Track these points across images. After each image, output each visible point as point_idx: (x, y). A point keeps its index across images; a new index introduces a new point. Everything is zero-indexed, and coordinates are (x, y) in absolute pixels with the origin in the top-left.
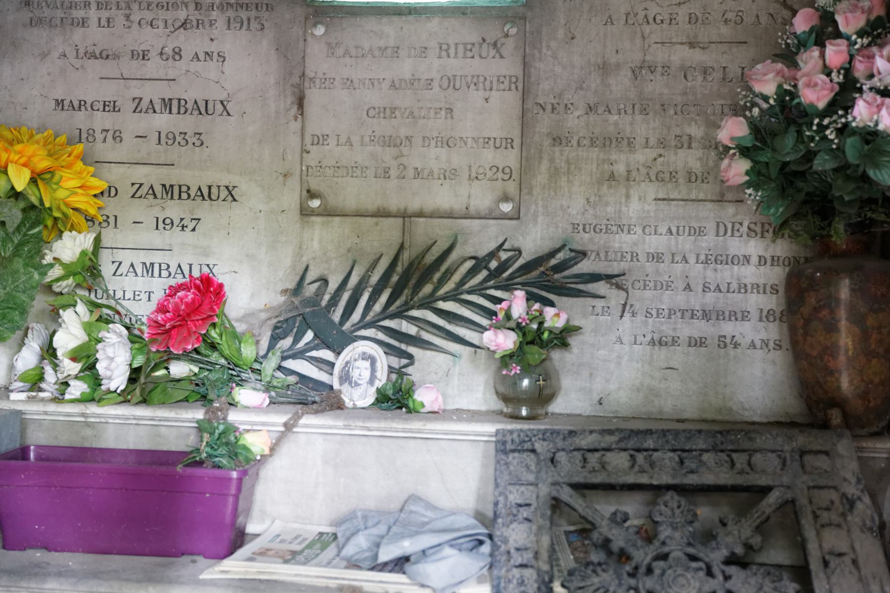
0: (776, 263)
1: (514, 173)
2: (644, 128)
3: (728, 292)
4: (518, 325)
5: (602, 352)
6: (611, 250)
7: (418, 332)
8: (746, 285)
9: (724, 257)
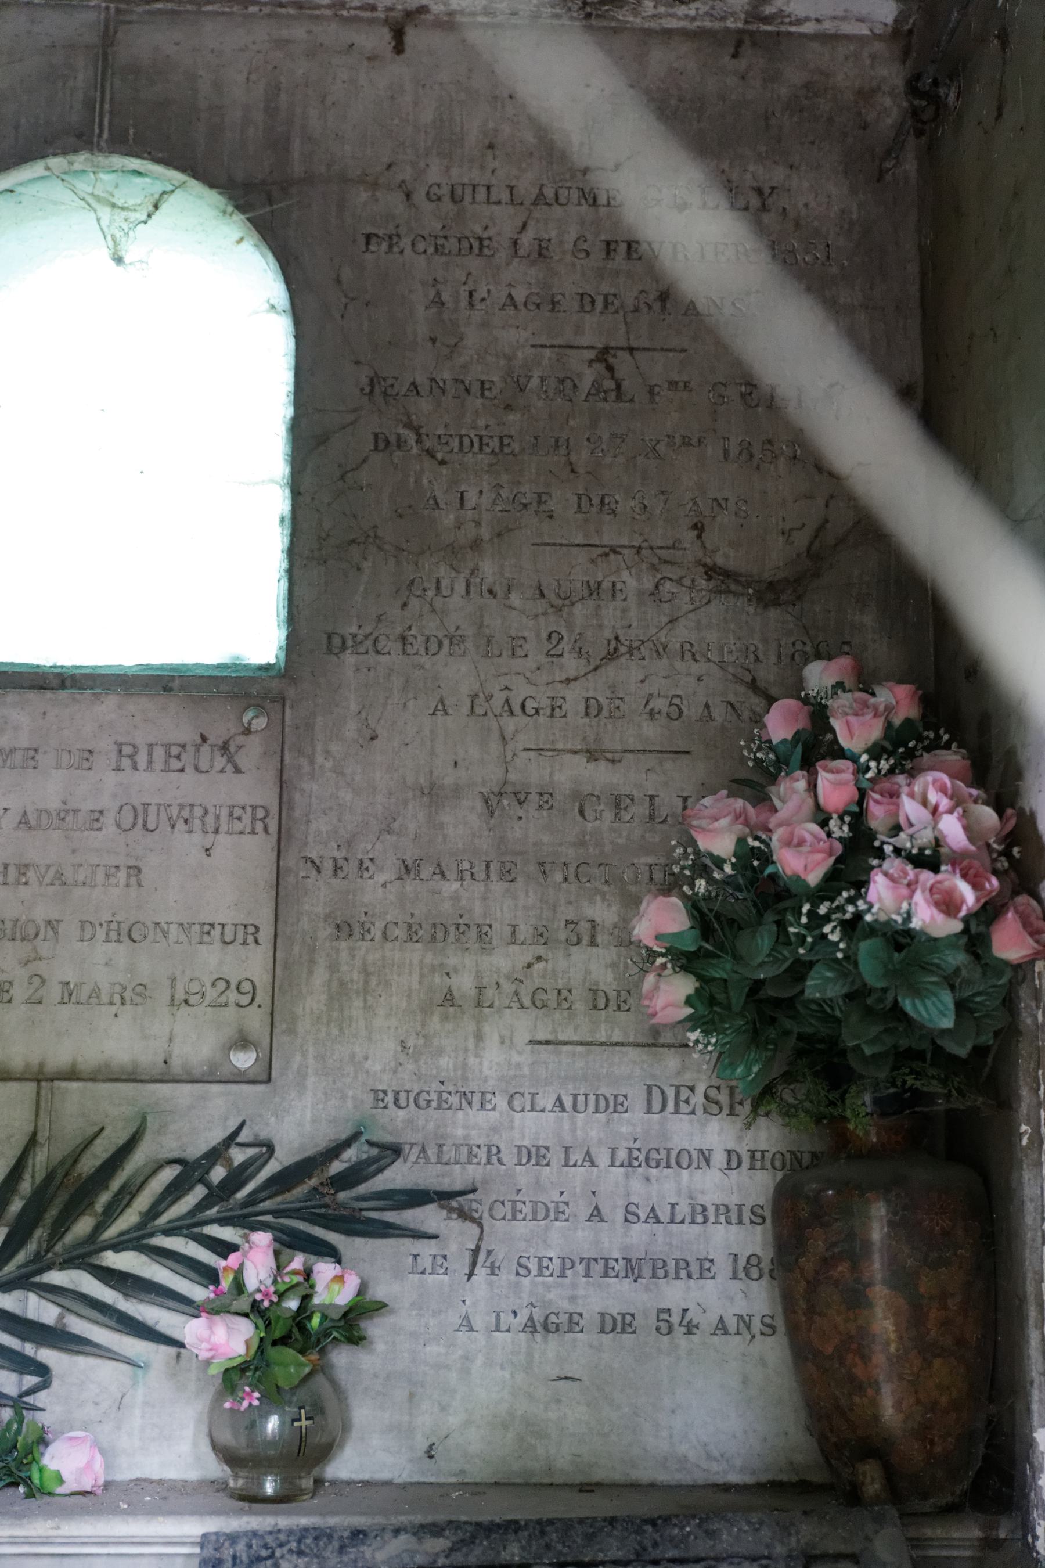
0: (758, 1164)
1: (259, 992)
2: (509, 906)
3: (672, 1221)
4: (255, 1305)
5: (433, 1349)
6: (449, 1142)
7: (61, 1317)
8: (705, 1209)
9: (663, 1154)
